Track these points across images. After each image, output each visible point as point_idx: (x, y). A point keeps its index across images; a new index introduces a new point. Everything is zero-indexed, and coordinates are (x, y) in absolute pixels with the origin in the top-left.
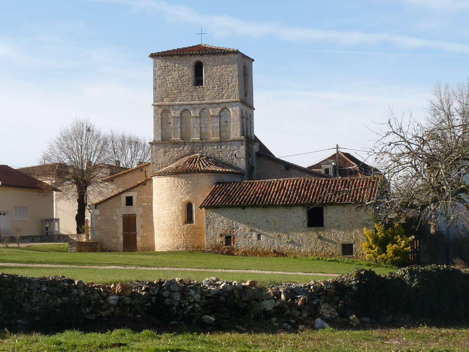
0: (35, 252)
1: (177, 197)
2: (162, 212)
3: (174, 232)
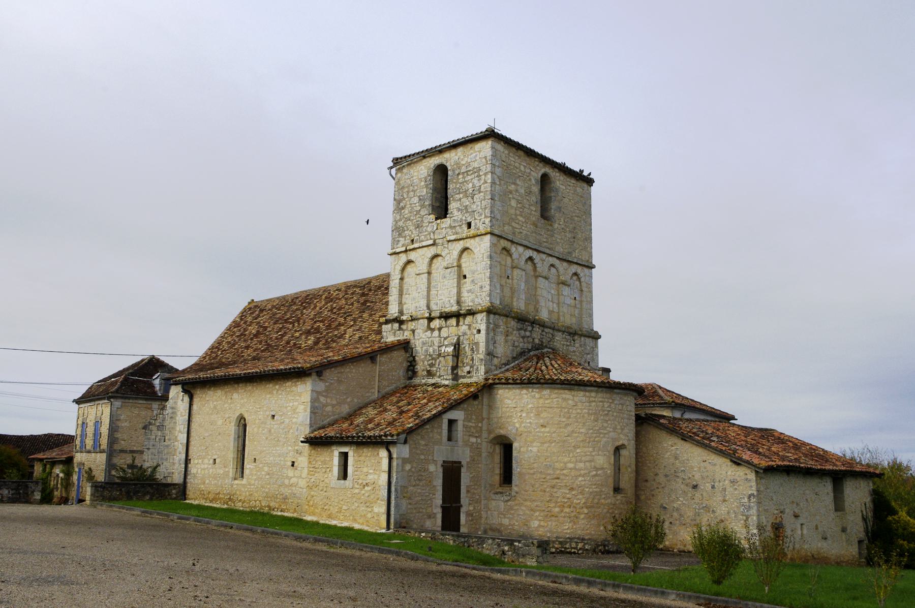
2: (571, 465)
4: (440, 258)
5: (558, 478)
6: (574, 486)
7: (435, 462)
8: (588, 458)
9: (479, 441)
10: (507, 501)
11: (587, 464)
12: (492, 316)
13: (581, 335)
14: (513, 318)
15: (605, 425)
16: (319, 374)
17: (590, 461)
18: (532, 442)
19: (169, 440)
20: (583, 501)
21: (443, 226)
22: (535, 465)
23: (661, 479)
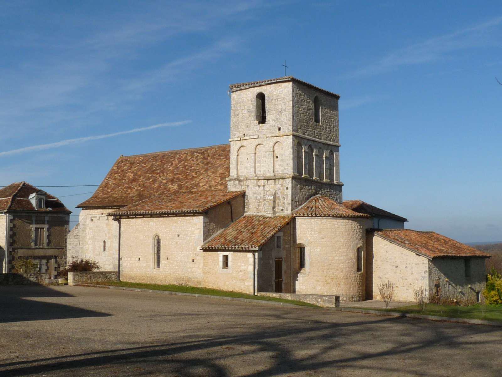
0: (42, 358)
1: (353, 242)
2: (336, 258)
3: (350, 280)
4: (261, 145)
5: (330, 265)
10: (304, 277)
19: (83, 244)
20: (343, 276)
21: (264, 128)
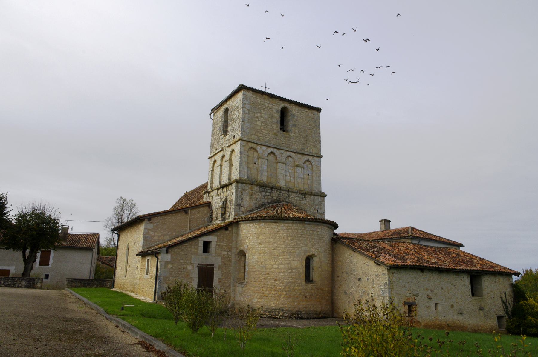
2: (275, 266)
6: (278, 278)
7: (192, 265)
8: (286, 262)
9: (229, 253)
11: (286, 266)
12: (240, 185)
13: (311, 195)
14: (257, 185)
15: (299, 243)
16: (149, 220)
17: (287, 264)
18: (255, 253)
20: (283, 287)
22: (256, 267)
23: (345, 275)
